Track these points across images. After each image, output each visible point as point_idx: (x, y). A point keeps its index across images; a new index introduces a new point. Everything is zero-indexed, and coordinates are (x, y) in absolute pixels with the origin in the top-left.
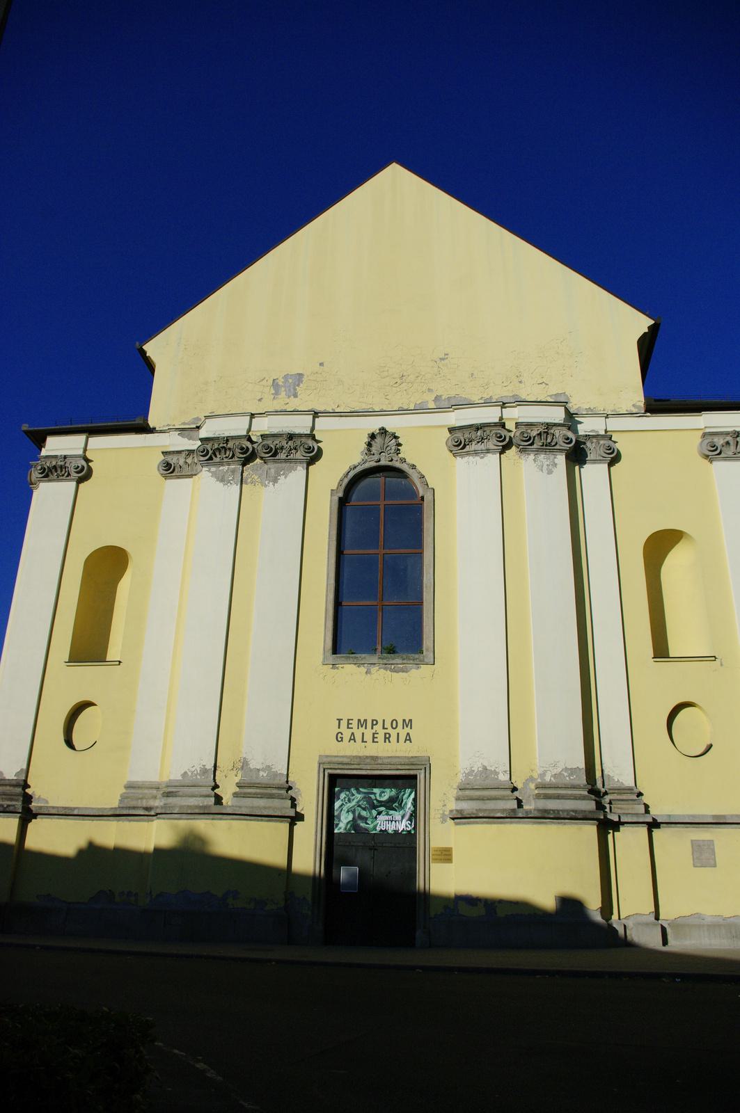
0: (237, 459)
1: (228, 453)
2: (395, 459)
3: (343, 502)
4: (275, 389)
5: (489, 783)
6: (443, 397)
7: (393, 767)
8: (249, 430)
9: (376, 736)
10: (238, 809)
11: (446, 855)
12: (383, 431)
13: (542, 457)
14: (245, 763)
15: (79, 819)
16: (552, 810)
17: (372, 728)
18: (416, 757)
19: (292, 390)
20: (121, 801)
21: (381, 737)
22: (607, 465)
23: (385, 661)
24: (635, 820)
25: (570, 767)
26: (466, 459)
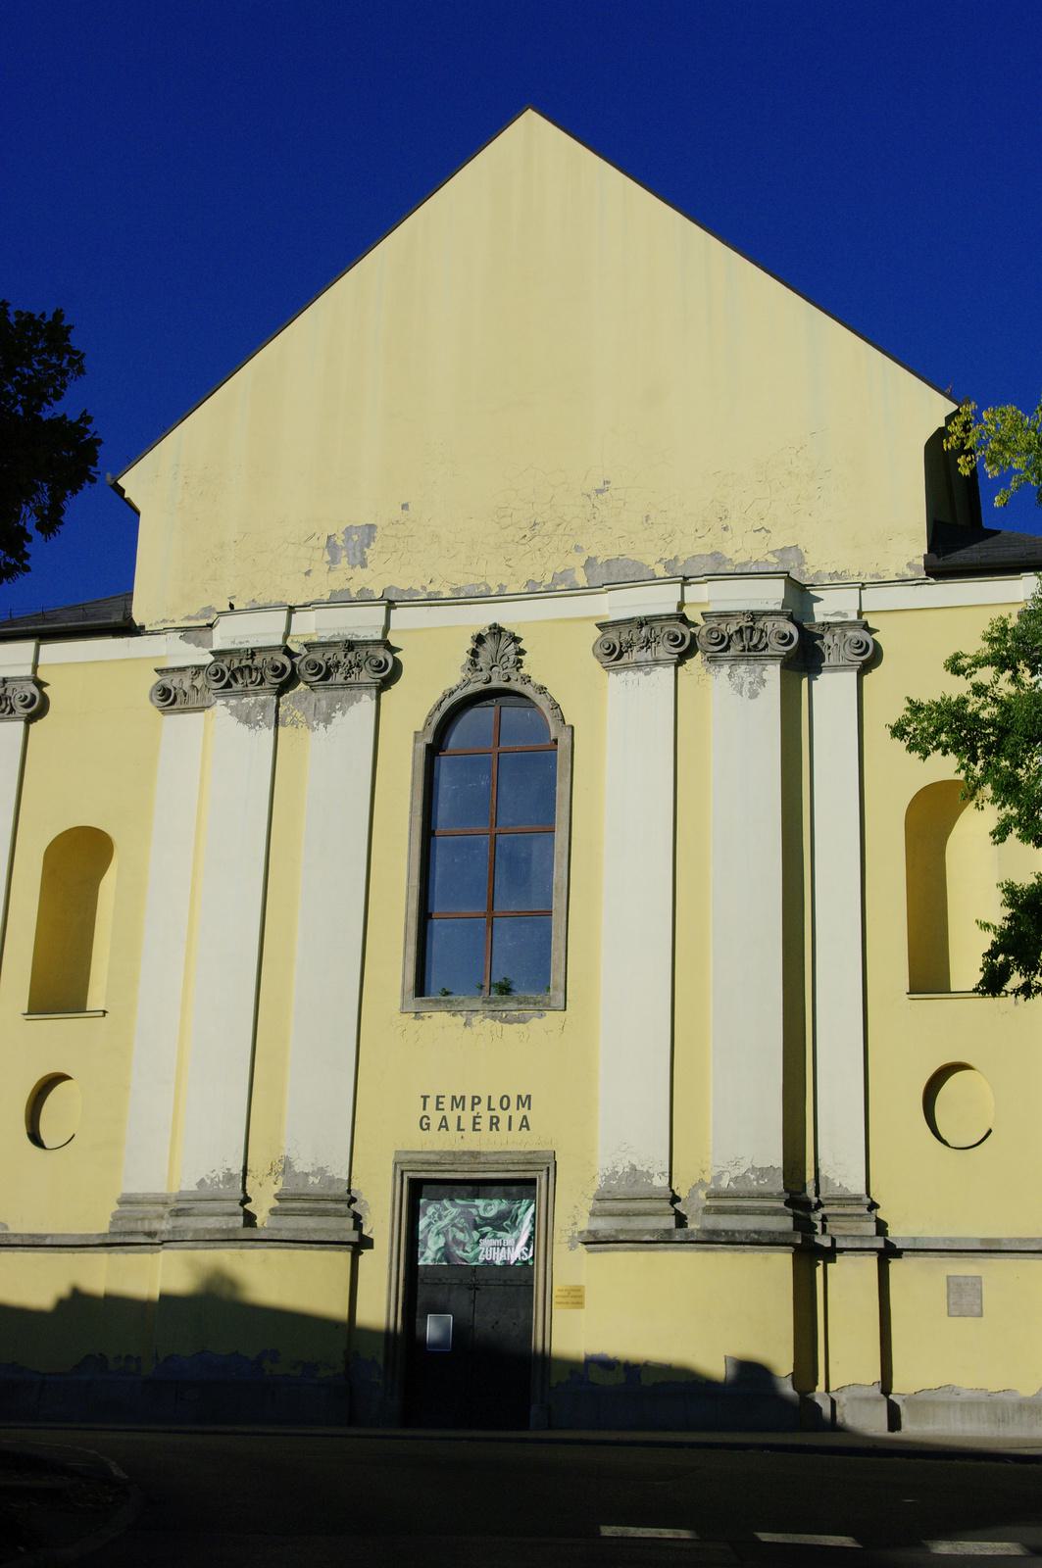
0: (269, 686)
1: (254, 674)
2: (513, 678)
3: (434, 752)
4: (331, 553)
5: (639, 1190)
6: (599, 561)
7: (501, 1167)
8: (287, 635)
9: (478, 1120)
10: (276, 1232)
11: (575, 1297)
12: (497, 631)
13: (742, 669)
14: (287, 1164)
15: (53, 1252)
16: (724, 1231)
17: (473, 1110)
18: (535, 1152)
19: (358, 554)
20: (112, 1224)
21: (484, 1123)
22: (855, 674)
23: (493, 1007)
24: (858, 1245)
25: (759, 1167)
26: (623, 676)
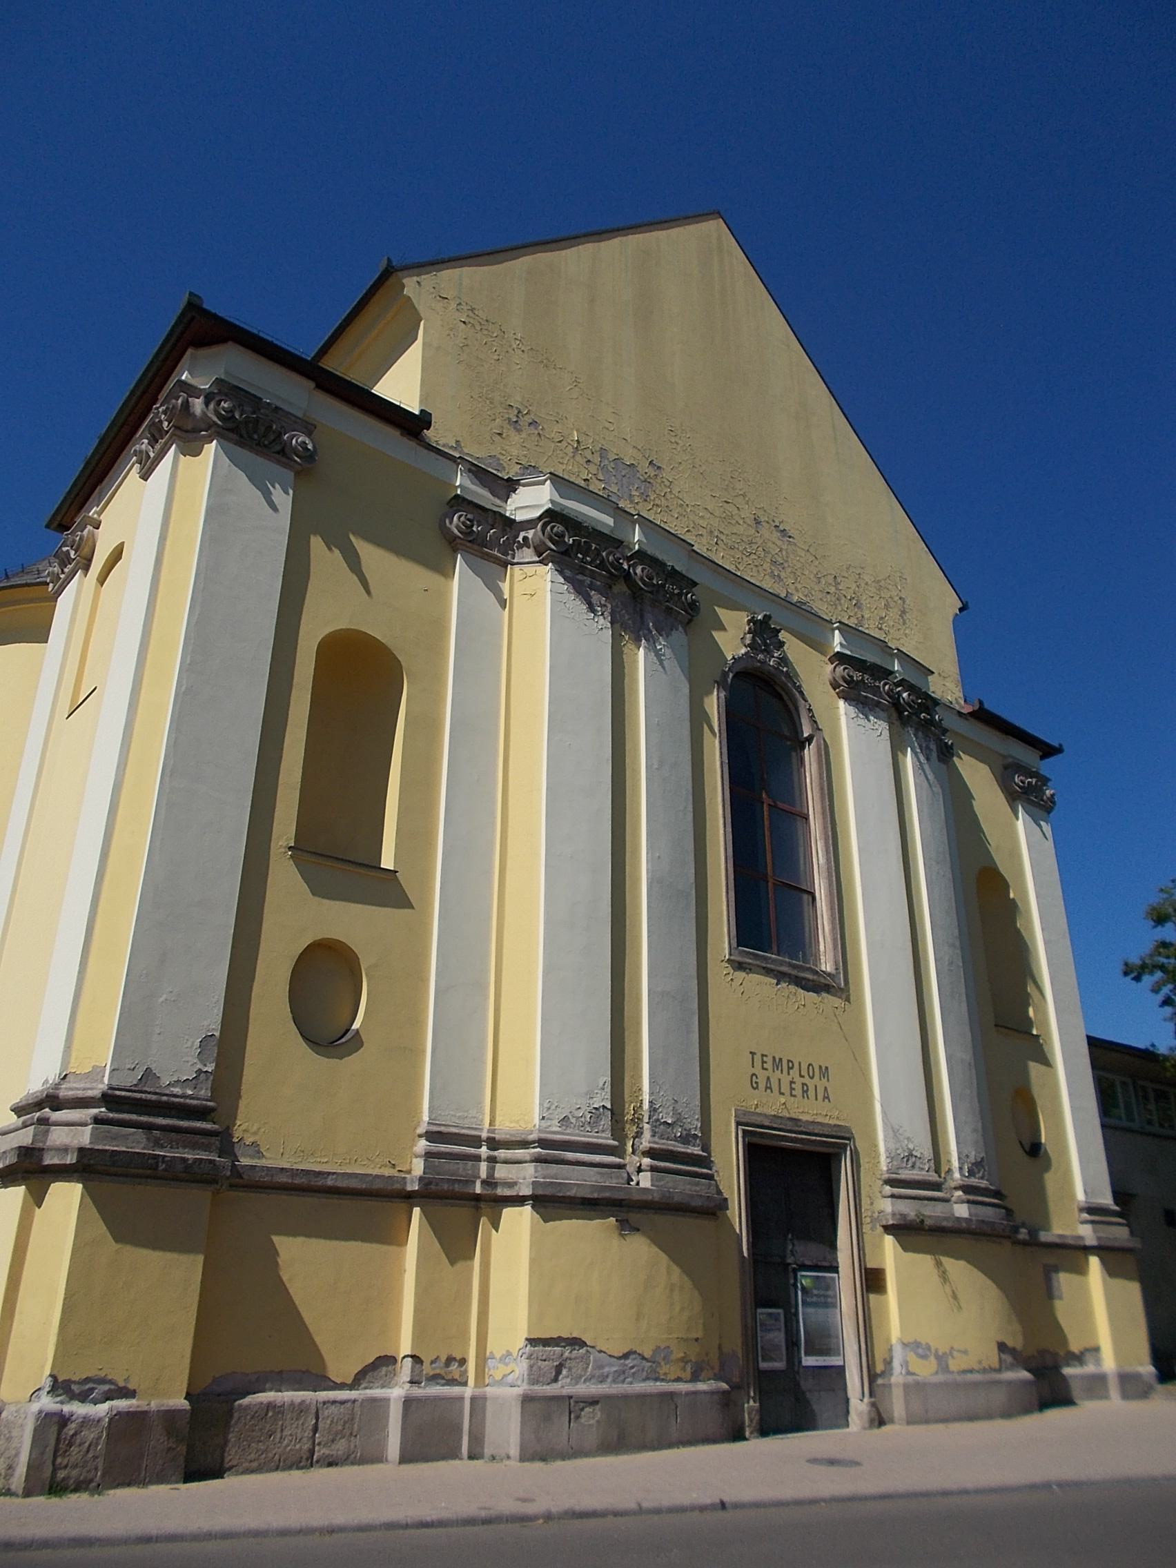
17: (789, 1074)
